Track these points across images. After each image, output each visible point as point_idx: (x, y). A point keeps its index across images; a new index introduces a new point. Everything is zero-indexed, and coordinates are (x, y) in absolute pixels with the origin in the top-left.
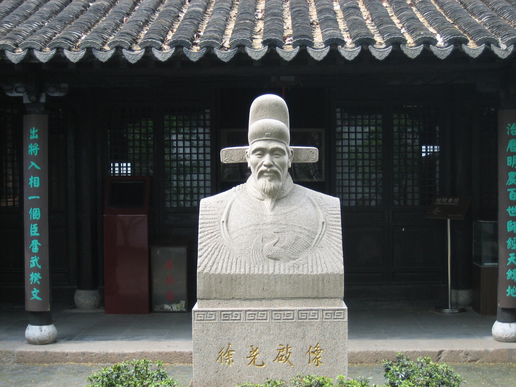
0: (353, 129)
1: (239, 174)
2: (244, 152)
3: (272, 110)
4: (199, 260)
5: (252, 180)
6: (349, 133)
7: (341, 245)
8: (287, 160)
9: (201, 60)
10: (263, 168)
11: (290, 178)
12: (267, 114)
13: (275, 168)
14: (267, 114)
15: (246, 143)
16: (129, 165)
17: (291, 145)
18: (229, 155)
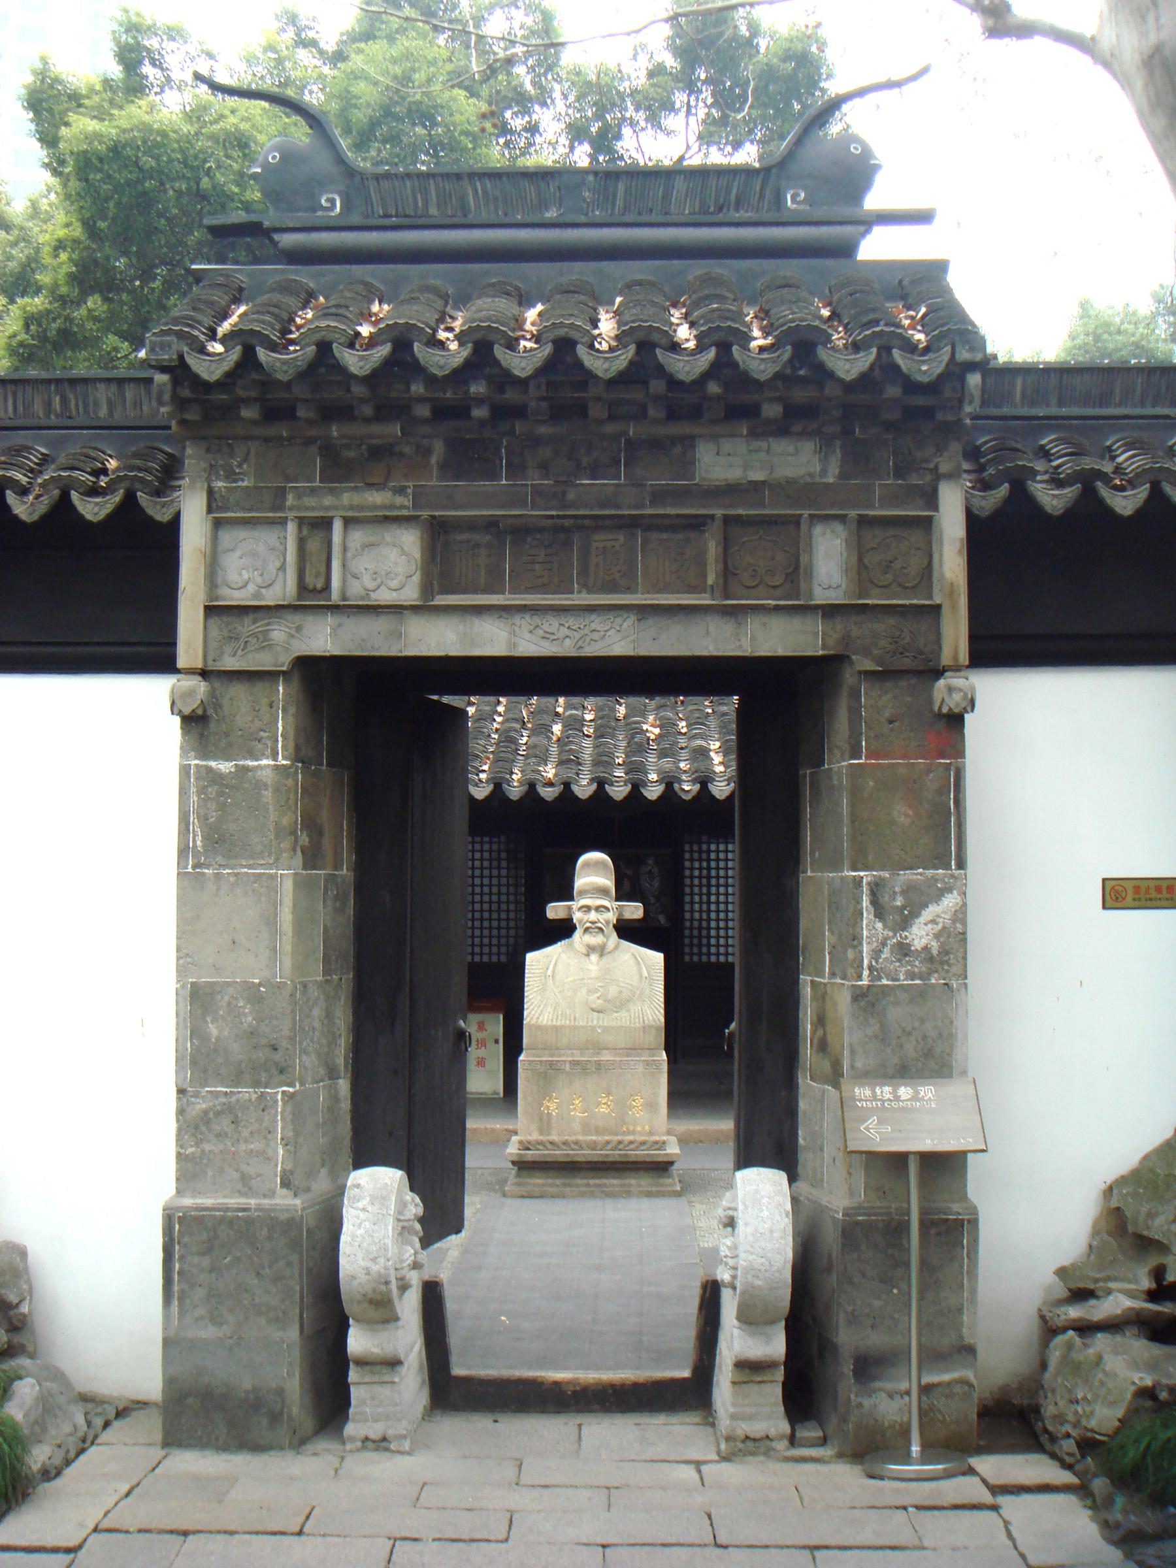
0: (722, 847)
1: (564, 929)
2: (570, 908)
3: (596, 866)
4: (525, 1013)
5: (577, 935)
6: (718, 851)
7: (662, 1000)
8: (612, 917)
9: (521, 798)
10: (588, 925)
11: (615, 934)
12: (594, 872)
13: (600, 925)
14: (594, 872)
15: (571, 898)
16: (687, 958)
17: (617, 900)
18: (555, 910)
